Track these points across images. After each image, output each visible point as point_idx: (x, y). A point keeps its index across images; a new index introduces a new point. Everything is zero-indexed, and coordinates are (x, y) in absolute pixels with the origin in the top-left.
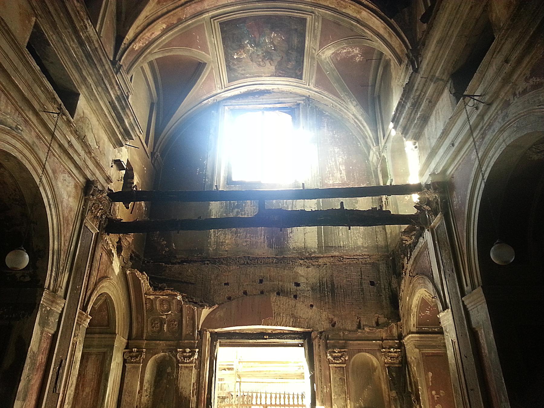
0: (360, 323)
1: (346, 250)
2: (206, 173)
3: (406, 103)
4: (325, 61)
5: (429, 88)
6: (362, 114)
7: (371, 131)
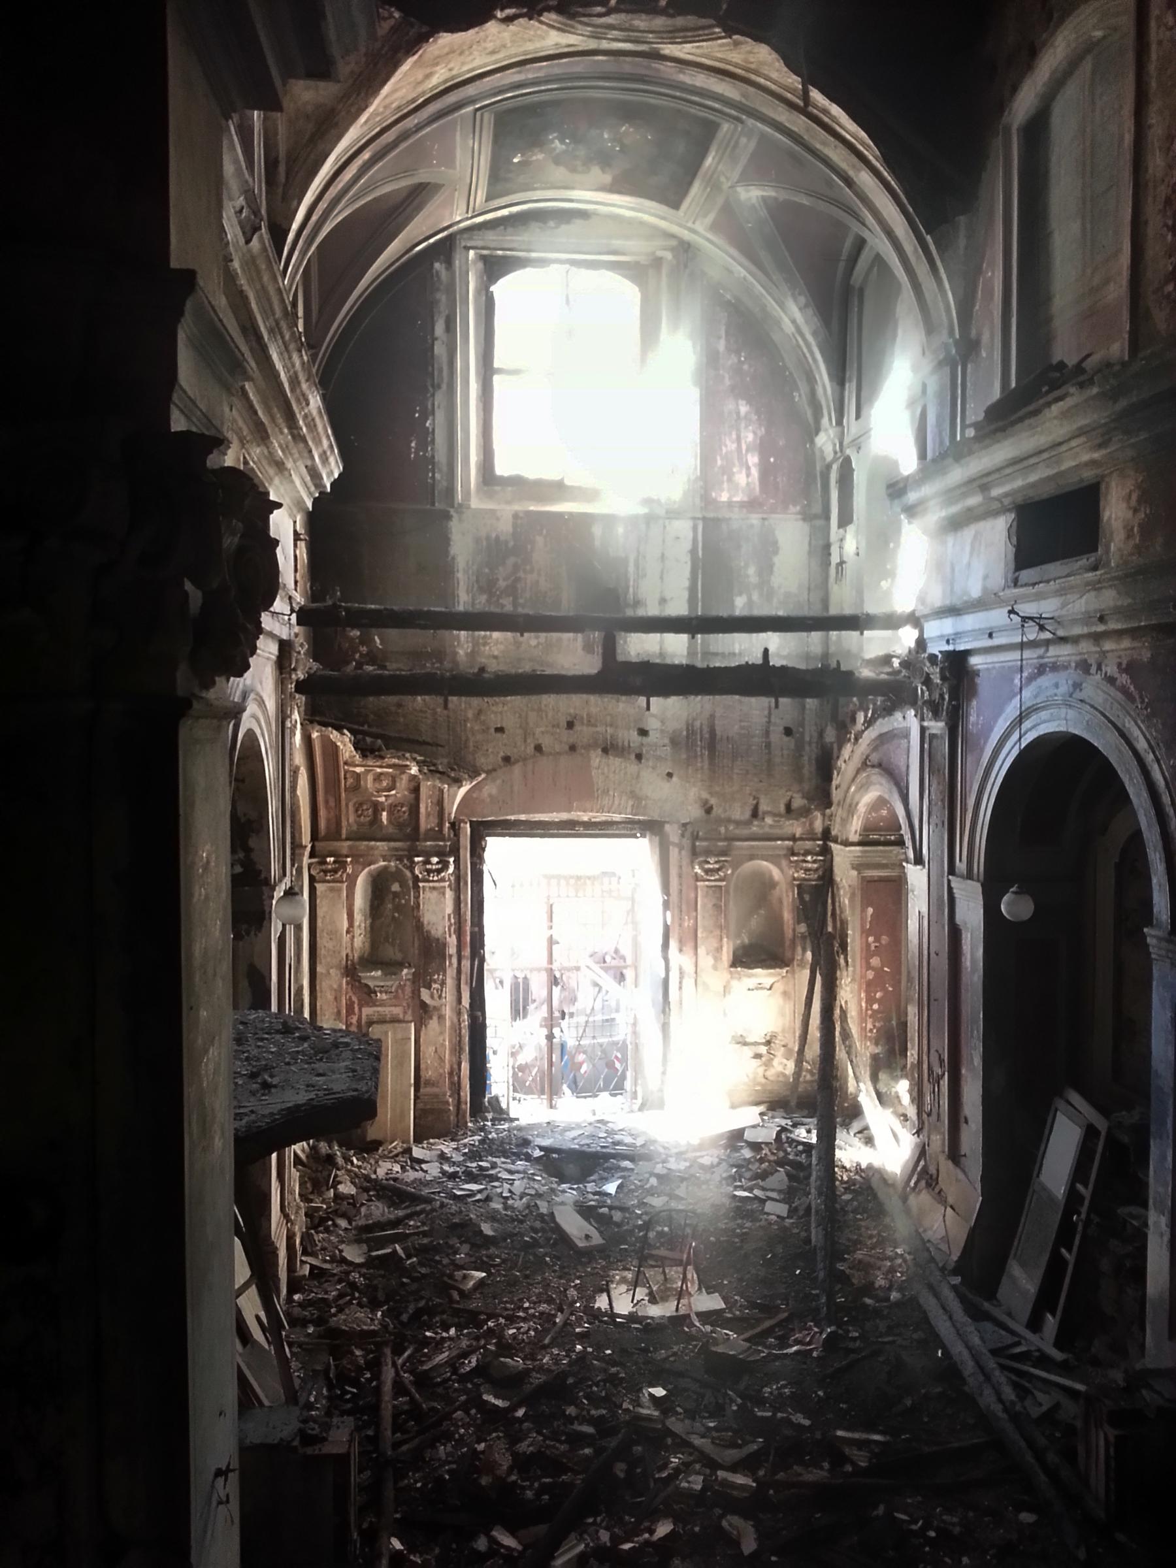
2: (433, 457)
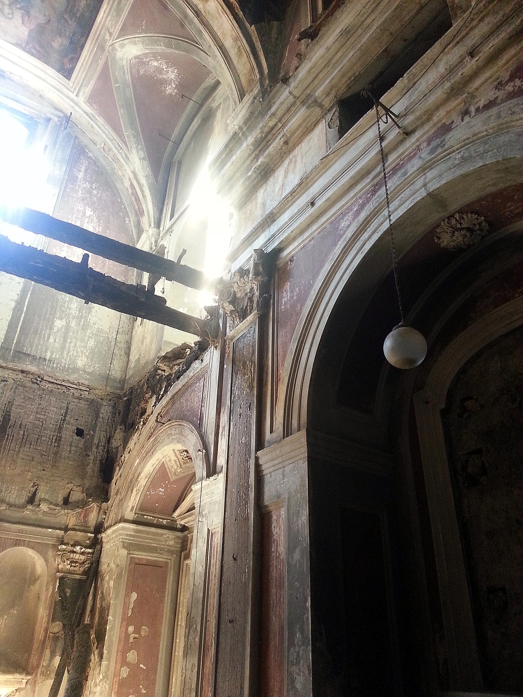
0: (34, 494)
1: (53, 367)
3: (246, 138)
4: (120, 62)
5: (294, 117)
6: (147, 176)
7: (153, 206)
